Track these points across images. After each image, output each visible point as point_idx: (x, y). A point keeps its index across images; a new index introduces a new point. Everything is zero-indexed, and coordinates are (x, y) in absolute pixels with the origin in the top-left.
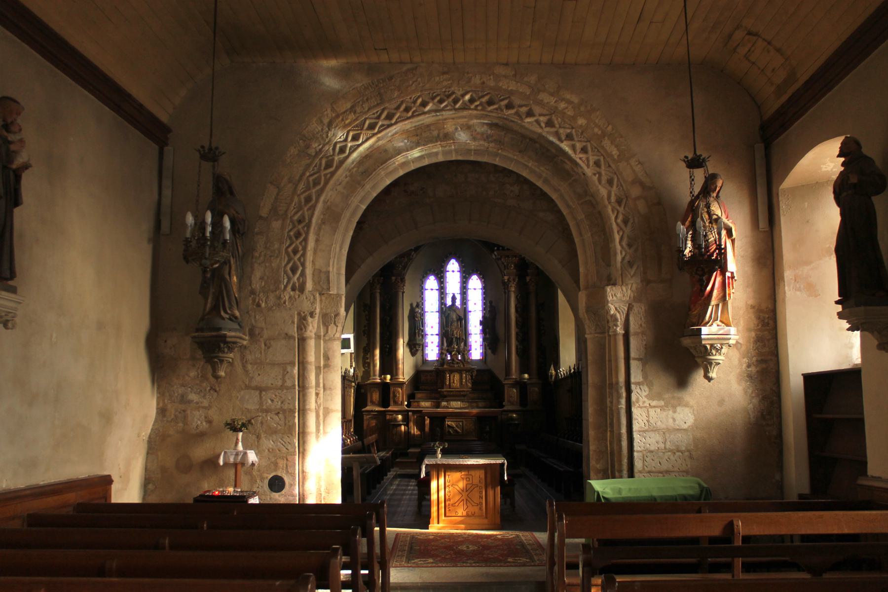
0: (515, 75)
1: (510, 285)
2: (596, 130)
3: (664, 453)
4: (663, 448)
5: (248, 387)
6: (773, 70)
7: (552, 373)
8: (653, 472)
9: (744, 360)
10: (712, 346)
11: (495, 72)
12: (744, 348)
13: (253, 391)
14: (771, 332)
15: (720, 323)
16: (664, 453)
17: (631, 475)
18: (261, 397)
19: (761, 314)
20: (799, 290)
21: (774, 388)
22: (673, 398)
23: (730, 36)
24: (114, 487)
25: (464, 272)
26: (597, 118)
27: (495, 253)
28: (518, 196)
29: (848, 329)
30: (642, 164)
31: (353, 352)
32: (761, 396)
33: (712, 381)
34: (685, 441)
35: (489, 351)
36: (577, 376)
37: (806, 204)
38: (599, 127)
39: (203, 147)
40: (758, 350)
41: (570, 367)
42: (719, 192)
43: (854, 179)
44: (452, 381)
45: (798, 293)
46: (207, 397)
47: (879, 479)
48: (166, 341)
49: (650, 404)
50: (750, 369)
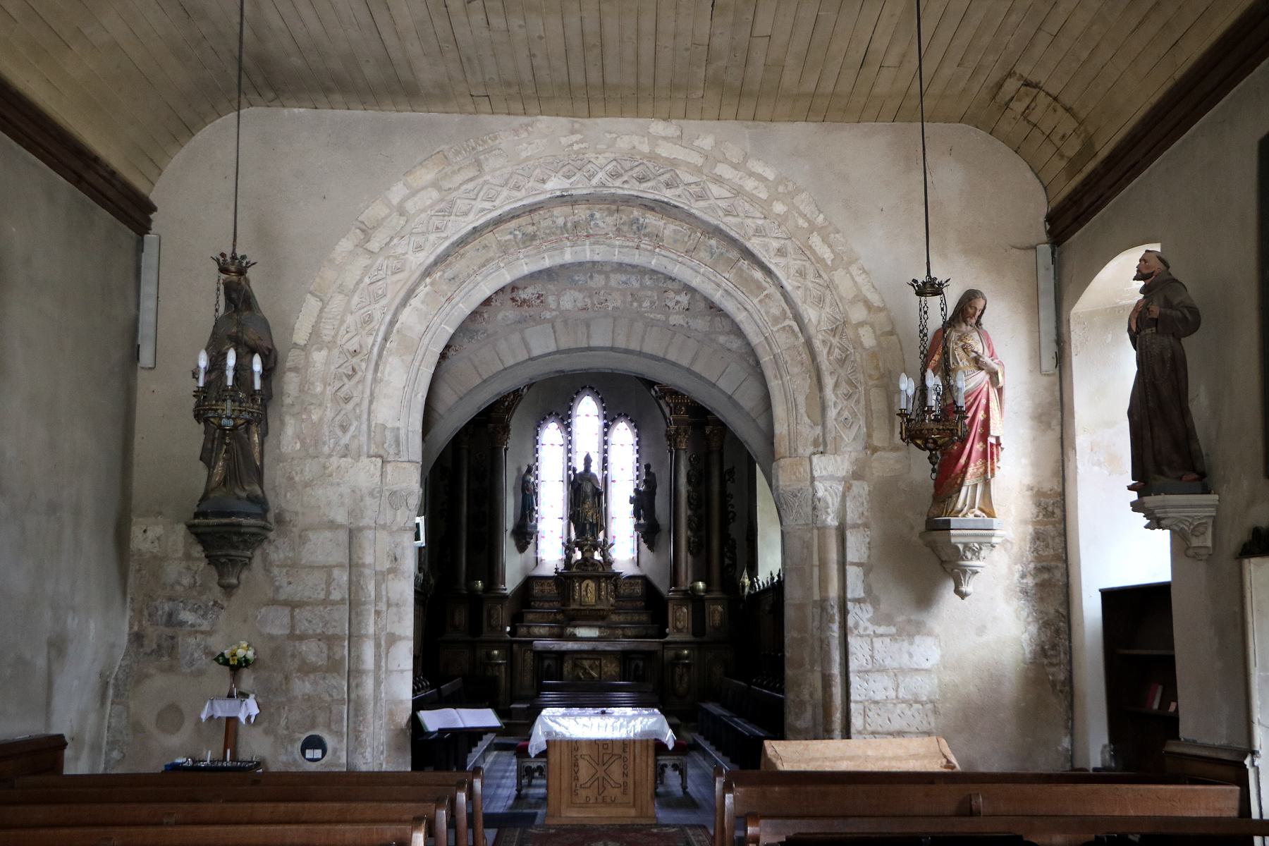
0: (680, 137)
1: (679, 440)
2: (801, 222)
3: (895, 704)
4: (894, 697)
5: (274, 602)
6: (1064, 136)
7: (744, 583)
8: (878, 733)
9: (1017, 567)
10: (966, 545)
11: (651, 131)
12: (1015, 549)
13: (279, 608)
14: (1057, 525)
15: (978, 512)
16: (895, 704)
17: (847, 734)
18: (292, 617)
19: (1042, 499)
20: (1099, 464)
21: (1061, 610)
22: (909, 621)
23: (1000, 85)
24: (68, 753)
25: (605, 417)
26: (803, 201)
28: (687, 309)
29: (1146, 527)
30: (867, 274)
31: (424, 545)
32: (1041, 622)
33: (967, 598)
34: (927, 686)
35: (644, 547)
36: (777, 588)
37: (1110, 336)
39: (223, 255)
40: (1037, 553)
41: (771, 574)
42: (980, 317)
43: (1155, 310)
44: (584, 593)
45: (1096, 468)
46: (209, 616)
47: (1193, 743)
48: (145, 531)
49: (874, 632)
50: (1025, 581)
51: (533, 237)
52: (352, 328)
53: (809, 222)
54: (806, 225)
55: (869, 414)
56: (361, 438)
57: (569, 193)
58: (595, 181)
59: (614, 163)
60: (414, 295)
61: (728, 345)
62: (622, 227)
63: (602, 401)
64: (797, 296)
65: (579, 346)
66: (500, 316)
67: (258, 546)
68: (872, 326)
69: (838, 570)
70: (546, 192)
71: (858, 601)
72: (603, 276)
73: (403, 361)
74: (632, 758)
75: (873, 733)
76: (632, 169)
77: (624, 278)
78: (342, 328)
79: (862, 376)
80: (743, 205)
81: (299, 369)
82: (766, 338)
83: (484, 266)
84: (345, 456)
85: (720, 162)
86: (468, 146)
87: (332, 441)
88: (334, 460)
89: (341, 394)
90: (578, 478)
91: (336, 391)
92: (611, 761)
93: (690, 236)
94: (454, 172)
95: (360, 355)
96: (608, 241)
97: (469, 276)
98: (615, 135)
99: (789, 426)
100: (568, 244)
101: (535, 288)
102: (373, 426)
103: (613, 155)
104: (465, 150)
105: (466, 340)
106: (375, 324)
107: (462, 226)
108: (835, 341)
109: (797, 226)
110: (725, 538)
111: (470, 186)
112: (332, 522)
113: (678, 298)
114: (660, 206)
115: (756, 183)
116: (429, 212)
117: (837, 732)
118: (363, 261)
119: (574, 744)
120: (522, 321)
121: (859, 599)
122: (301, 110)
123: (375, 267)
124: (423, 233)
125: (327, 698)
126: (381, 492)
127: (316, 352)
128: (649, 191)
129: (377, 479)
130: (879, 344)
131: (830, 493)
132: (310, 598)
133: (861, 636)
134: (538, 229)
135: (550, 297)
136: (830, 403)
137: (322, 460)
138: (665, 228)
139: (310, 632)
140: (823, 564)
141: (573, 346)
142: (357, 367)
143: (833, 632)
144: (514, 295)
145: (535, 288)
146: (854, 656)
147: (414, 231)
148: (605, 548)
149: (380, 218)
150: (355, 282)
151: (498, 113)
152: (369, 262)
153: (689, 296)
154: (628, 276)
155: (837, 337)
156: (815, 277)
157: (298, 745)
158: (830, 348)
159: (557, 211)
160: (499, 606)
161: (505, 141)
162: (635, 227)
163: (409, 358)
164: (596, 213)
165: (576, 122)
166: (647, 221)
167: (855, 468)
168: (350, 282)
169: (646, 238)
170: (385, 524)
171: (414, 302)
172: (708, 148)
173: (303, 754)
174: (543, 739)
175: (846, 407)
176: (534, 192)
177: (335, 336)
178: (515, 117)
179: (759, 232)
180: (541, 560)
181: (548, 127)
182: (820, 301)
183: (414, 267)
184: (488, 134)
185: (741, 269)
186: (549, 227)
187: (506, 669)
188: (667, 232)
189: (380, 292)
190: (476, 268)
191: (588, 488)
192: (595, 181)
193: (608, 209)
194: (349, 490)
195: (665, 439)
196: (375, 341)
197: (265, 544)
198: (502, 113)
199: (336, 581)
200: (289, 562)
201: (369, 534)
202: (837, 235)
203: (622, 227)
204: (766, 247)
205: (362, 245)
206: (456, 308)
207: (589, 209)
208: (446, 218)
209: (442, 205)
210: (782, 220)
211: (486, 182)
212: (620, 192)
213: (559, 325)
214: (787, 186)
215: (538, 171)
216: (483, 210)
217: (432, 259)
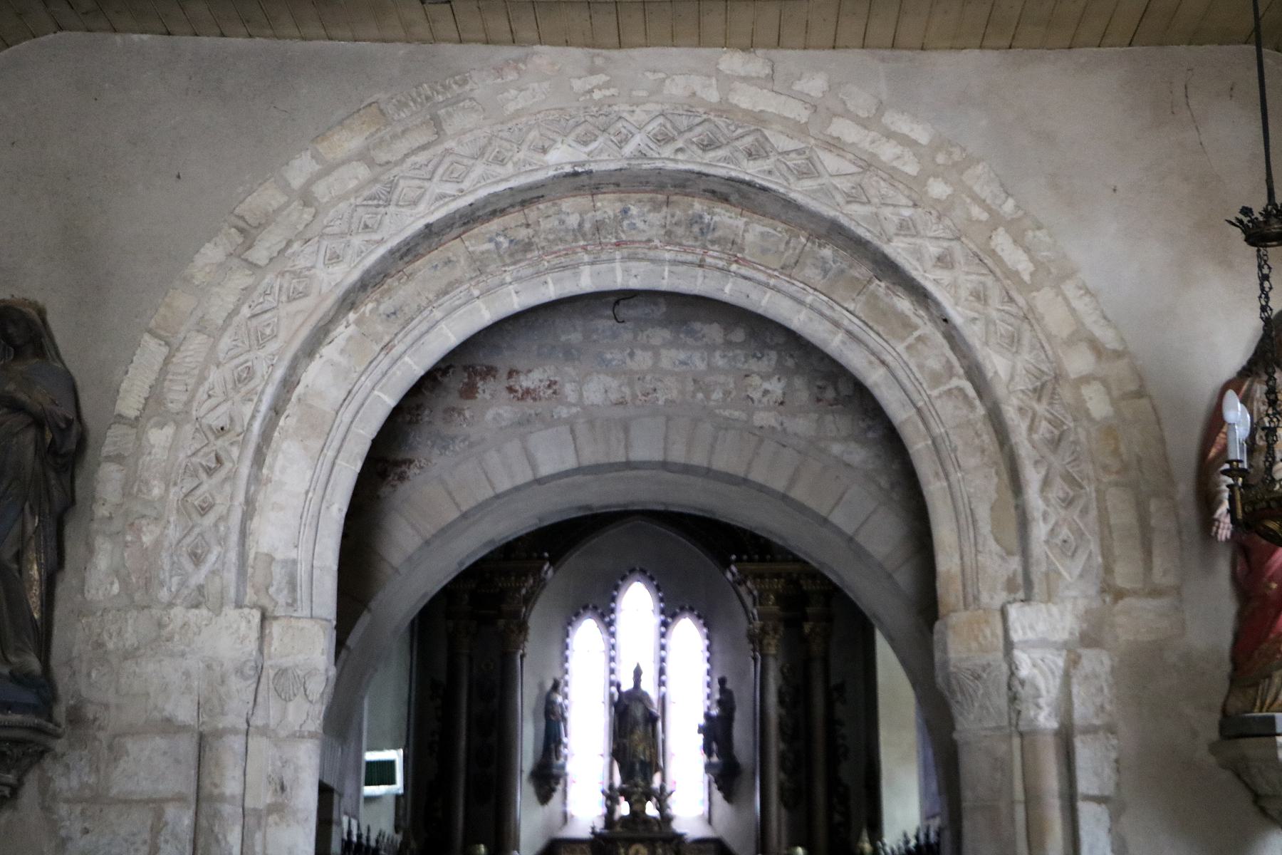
0: (771, 78)
2: (977, 212)
25: (663, 612)
26: (978, 178)
27: (733, 568)
28: (782, 403)
30: (1092, 295)
31: (401, 791)
35: (718, 796)
38: (982, 202)
51: (528, 246)
52: (218, 390)
53: (988, 209)
54: (984, 216)
56: (226, 575)
57: (587, 168)
58: (629, 149)
59: (661, 120)
60: (328, 340)
61: (846, 458)
63: (658, 588)
64: (973, 334)
65: (612, 460)
66: (490, 414)
67: (31, 765)
68: (1104, 381)
69: (1063, 809)
70: (548, 167)
72: (650, 353)
73: (306, 448)
76: (690, 129)
77: (682, 355)
78: (201, 390)
80: (877, 186)
81: (124, 457)
82: (919, 410)
83: (446, 293)
84: (197, 606)
85: (835, 115)
86: (419, 95)
87: (175, 580)
88: (178, 612)
89: (195, 500)
90: (624, 697)
91: (186, 495)
93: (788, 243)
94: (395, 137)
95: (229, 436)
96: (652, 254)
97: (420, 310)
98: (662, 75)
99: (962, 558)
100: (586, 258)
102: (252, 556)
103: (659, 108)
104: (414, 101)
105: (436, 451)
106: (257, 382)
107: (408, 222)
108: (1041, 408)
109: (970, 219)
110: (833, 783)
111: (421, 158)
112: (168, 720)
113: (767, 386)
114: (739, 191)
115: (898, 150)
116: (352, 200)
118: (241, 279)
120: (524, 422)
122: (145, 37)
123: (260, 290)
124: (342, 235)
126: (259, 671)
127: (154, 430)
128: (719, 165)
129: (252, 646)
131: (1042, 672)
134: (536, 233)
137: (156, 612)
138: (745, 231)
140: (1033, 799)
141: (602, 459)
142: (223, 455)
145: (545, 371)
147: (328, 230)
148: (662, 798)
149: (271, 210)
150: (225, 314)
151: (468, 41)
152: (249, 281)
153: (783, 383)
154: (689, 353)
155: (1045, 401)
156: (1003, 303)
158: (1033, 421)
159: (567, 204)
161: (481, 86)
162: (696, 229)
163: (316, 444)
164: (632, 207)
165: (598, 55)
166: (716, 218)
167: (1085, 626)
168: (217, 314)
169: (716, 247)
170: (266, 726)
171: (328, 351)
175: (1065, 520)
176: (528, 168)
177: (188, 403)
178: (498, 47)
179: (905, 227)
180: (572, 816)
181: (553, 64)
182: (1014, 341)
183: (324, 290)
184: (452, 76)
185: (874, 296)
186: (551, 231)
188: (750, 237)
189: (268, 331)
190: (431, 296)
191: (638, 712)
192: (629, 149)
193: (651, 200)
194: (201, 665)
195: (746, 641)
196: (256, 411)
197: (47, 761)
198: (476, 41)
199: (170, 827)
200: (87, 793)
201: (236, 743)
202: (1038, 233)
204: (918, 253)
205: (240, 255)
206: (399, 363)
207: (621, 200)
208: (382, 210)
209: (377, 188)
210: (942, 210)
211: (448, 152)
212: (670, 166)
213: (581, 427)
214: (950, 154)
215: (534, 134)
217: (355, 276)
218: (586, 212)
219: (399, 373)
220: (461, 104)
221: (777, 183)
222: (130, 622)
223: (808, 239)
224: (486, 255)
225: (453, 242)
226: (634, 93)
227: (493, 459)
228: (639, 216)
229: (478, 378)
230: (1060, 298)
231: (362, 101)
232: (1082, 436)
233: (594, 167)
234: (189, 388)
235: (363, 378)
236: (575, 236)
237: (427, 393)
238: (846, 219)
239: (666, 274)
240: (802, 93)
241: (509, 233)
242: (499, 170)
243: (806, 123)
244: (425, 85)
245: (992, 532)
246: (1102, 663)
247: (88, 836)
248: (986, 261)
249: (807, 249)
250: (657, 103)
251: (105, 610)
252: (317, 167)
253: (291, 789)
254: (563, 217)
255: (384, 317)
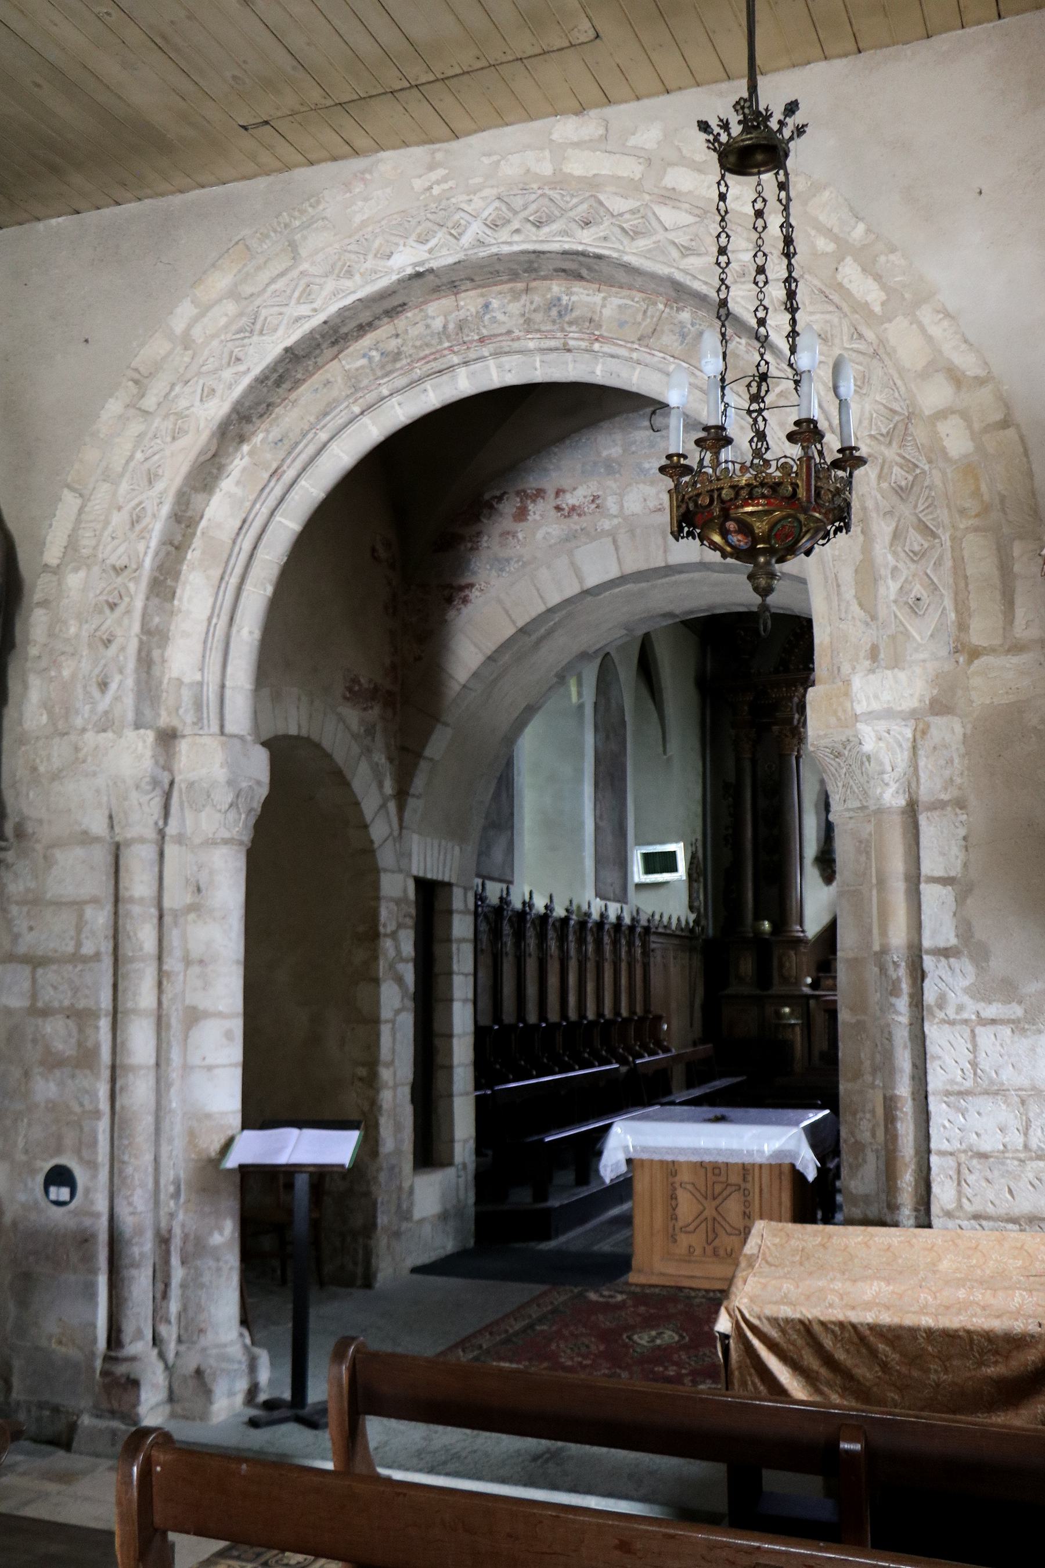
0: (605, 138)
4: (1020, 1147)
8: (988, 1218)
11: (554, 137)
18: (34, 981)
51: (397, 356)
53: (835, 238)
54: (831, 247)
55: (962, 584)
57: (427, 266)
58: (466, 240)
60: (225, 475)
62: (534, 316)
65: (652, 566)
66: (539, 535)
68: (964, 415)
71: (945, 953)
74: (757, 1190)
75: (976, 1217)
78: (106, 533)
79: (946, 511)
83: (325, 414)
84: (104, 731)
85: (671, 164)
86: (279, 223)
87: (88, 707)
88: (90, 736)
92: (725, 1194)
94: (259, 268)
96: (516, 345)
98: (495, 158)
100: (456, 360)
101: (588, 487)
103: (494, 192)
104: (275, 231)
105: (494, 573)
111: (279, 285)
112: (85, 833)
117: (906, 1213)
119: (671, 1166)
120: (571, 537)
121: (946, 949)
122: (60, 219)
125: (77, 1109)
130: (980, 448)
132: (56, 951)
133: (952, 1023)
135: (609, 498)
136: (883, 572)
137: (73, 737)
139: (56, 1004)
141: (643, 566)
143: (899, 1014)
144: (559, 502)
145: (588, 487)
146: (937, 1063)
150: (123, 461)
157: (40, 1179)
160: (792, 953)
165: (439, 150)
166: (574, 298)
167: (935, 692)
169: (574, 328)
172: (651, 145)
173: (47, 1192)
174: (621, 1157)
184: (308, 200)
186: (419, 337)
187: (802, 1030)
188: (607, 312)
190: (312, 419)
192: (466, 240)
193: (512, 290)
196: (148, 547)
202: (892, 257)
203: (534, 316)
207: (482, 295)
209: (244, 320)
212: (506, 249)
213: (623, 538)
216: (298, 319)
218: (451, 312)
219: (297, 497)
220: (315, 226)
221: (610, 248)
222: (56, 747)
223: (666, 305)
224: (360, 371)
225: (331, 364)
226: (471, 182)
227: (544, 574)
228: (499, 309)
229: (529, 502)
230: (914, 326)
231: (230, 240)
232: (938, 482)
233: (434, 264)
234: (97, 533)
235: (258, 506)
236: (440, 338)
237: (485, 521)
238: (682, 274)
239: (538, 364)
240: (635, 147)
241: (381, 345)
242: (348, 284)
243: (640, 179)
244: (285, 214)
245: (856, 597)
246: (953, 732)
247: (33, 933)
248: (831, 297)
249: (664, 315)
250: (492, 187)
251: (38, 738)
252: (196, 311)
253: (207, 889)
254: (429, 321)
255: (272, 445)
